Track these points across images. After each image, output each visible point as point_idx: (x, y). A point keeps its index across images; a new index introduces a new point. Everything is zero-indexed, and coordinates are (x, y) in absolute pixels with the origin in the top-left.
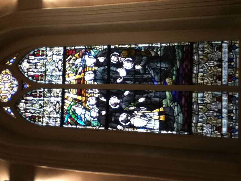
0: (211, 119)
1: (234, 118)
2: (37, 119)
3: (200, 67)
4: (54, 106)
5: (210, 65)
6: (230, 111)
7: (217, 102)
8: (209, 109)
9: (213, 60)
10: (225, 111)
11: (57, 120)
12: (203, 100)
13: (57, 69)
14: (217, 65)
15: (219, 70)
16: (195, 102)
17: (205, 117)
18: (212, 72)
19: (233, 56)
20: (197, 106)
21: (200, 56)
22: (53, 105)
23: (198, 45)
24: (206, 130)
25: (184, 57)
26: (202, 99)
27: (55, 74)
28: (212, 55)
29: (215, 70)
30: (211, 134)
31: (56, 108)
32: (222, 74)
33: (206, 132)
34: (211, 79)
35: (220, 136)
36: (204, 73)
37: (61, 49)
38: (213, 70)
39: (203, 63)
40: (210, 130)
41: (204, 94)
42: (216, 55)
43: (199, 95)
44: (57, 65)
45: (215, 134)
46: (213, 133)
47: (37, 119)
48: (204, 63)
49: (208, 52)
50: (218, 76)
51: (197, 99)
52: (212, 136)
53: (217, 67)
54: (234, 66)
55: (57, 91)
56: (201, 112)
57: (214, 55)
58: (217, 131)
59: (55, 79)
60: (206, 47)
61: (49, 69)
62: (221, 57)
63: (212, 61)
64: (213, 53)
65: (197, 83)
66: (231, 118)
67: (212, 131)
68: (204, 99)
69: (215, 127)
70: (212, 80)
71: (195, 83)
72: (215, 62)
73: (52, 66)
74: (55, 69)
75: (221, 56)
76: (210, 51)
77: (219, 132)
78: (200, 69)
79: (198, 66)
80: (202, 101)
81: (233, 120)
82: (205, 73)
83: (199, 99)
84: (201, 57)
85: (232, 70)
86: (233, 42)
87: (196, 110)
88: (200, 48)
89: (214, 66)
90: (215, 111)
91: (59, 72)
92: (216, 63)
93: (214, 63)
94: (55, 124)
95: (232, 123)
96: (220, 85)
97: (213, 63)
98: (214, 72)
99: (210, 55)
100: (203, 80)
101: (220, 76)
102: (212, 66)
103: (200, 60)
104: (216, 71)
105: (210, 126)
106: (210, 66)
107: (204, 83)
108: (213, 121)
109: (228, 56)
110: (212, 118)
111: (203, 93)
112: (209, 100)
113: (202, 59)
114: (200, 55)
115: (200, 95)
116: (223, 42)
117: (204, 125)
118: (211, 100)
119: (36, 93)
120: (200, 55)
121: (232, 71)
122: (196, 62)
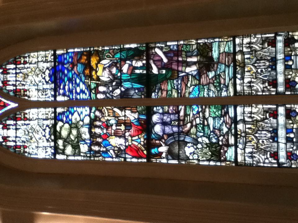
0: (263, 142)
1: (294, 140)
2: (22, 148)
3: (246, 70)
4: (43, 75)
5: (260, 66)
6: (289, 131)
7: (271, 118)
8: (259, 58)
9: (265, 60)
10: (280, 56)
11: (47, 93)
12: (251, 47)
13: (44, 81)
14: (269, 67)
15: (275, 145)
16: (241, 120)
17: (255, 139)
18: (264, 148)
19: (291, 53)
20: (244, 125)
21: (246, 54)
22: (42, 73)
23: (243, 40)
24: (255, 86)
25: (223, 114)
26: (250, 84)
27: (42, 87)
28: (263, 124)
29: (267, 144)
30: (263, 91)
31: (45, 77)
32: (278, 150)
33: (258, 161)
34: (263, 157)
35: (276, 165)
36: (251, 78)
37: (50, 53)
38: (265, 145)
39: (251, 65)
40: (262, 86)
41: (251, 39)
42: (268, 124)
43: (244, 40)
44: (44, 76)
45: (269, 90)
46: (265, 89)
47: (22, 148)
48: (252, 65)
49: (257, 49)
50: (271, 81)
51: (245, 155)
52: (264, 94)
53: (270, 69)
54: (293, 67)
55: (46, 98)
56: (250, 134)
57: (267, 123)
58: (271, 87)
59: (42, 95)
60: (254, 42)
61: (34, 81)
62: (275, 55)
63: (263, 61)
64: (266, 121)
65: (244, 162)
66: (288, 67)
67: (264, 88)
68: (252, 84)
69: (269, 153)
70: (265, 159)
71: (241, 162)
72: (266, 63)
73: (38, 77)
74: (41, 81)
75: (275, 53)
76: (260, 47)
77: (273, 87)
78: (246, 60)
79: (244, 138)
80: (251, 159)
81: (292, 70)
82: (253, 78)
83: (246, 156)
84: (246, 56)
85: (291, 145)
86: (290, 33)
87: (243, 130)
88: (247, 153)
89: (266, 68)
90: (268, 60)
91: (47, 84)
92: (267, 64)
93: (266, 64)
94: (46, 98)
95: (291, 73)
96: (274, 93)
97: (265, 135)
98: (267, 147)
99: (261, 123)
100: (252, 157)
101: (275, 82)
102: (265, 138)
103: (247, 130)
104: (270, 145)
105: (261, 81)
106: (262, 139)
107: (254, 162)
108: (265, 74)
109: (285, 78)
110: (263, 69)
111: (249, 38)
112: (258, 46)
113: (248, 59)
114: (245, 53)
115: (246, 40)
116: (276, 35)
117: (253, 80)
118: (261, 46)
119: (20, 150)
120: (245, 53)
121: (292, 146)
122: (242, 133)
